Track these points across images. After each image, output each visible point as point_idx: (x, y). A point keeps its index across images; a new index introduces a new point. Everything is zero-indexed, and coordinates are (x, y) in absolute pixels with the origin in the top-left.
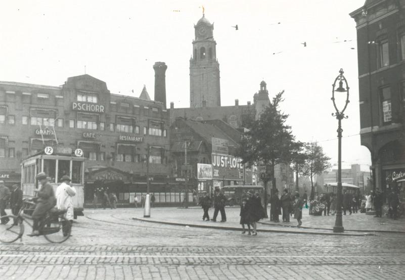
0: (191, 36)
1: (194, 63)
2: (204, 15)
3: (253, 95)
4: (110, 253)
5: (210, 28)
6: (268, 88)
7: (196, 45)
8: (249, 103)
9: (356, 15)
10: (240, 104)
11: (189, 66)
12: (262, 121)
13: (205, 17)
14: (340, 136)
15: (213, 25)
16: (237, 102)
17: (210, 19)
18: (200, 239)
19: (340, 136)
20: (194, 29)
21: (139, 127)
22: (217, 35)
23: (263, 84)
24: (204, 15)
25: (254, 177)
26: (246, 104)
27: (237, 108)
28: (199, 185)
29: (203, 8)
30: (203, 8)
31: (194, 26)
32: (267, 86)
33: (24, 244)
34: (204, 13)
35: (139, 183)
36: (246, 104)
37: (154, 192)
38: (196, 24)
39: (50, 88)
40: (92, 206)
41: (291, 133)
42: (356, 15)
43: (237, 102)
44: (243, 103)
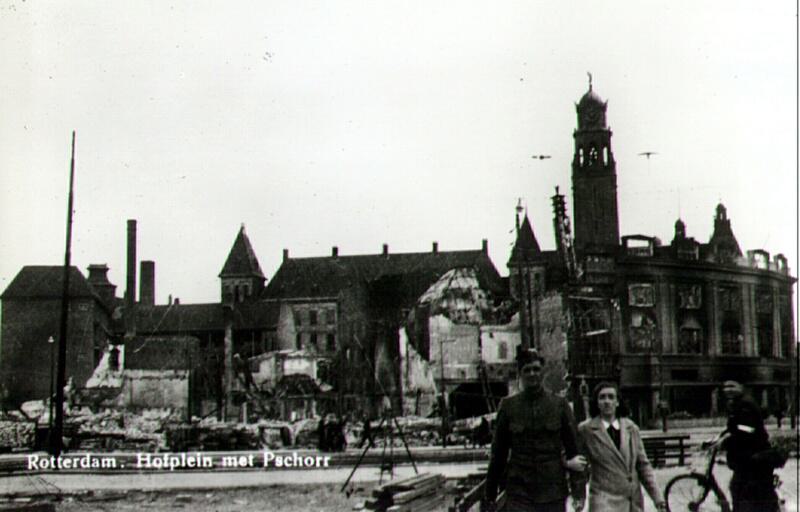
2: (591, 86)
14: (70, 221)
19: (70, 221)
24: (591, 86)
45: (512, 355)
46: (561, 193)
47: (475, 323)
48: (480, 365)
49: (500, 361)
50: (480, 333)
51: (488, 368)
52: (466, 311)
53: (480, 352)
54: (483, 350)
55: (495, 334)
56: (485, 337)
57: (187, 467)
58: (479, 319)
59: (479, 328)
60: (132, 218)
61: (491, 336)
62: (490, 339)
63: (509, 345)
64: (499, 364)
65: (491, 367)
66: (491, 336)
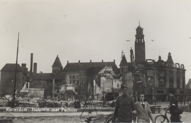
0: (67, 62)
2: (139, 25)
5: (142, 30)
7: (54, 68)
9: (186, 70)
11: (134, 45)
12: (153, 110)
14: (18, 39)
15: (143, 29)
17: (142, 26)
19: (18, 39)
22: (144, 33)
24: (139, 25)
34: (140, 24)
35: (139, 82)
37: (144, 97)
38: (136, 28)
40: (183, 79)
41: (40, 72)
42: (186, 70)
45: (120, 87)
46: (132, 49)
47: (112, 79)
48: (113, 89)
49: (117, 88)
50: (113, 81)
51: (114, 90)
52: (109, 76)
53: (113, 86)
54: (113, 85)
55: (116, 82)
56: (114, 82)
57: (43, 111)
58: (112, 78)
59: (112, 80)
60: (32, 53)
61: (115, 82)
62: (115, 83)
63: (119, 84)
64: (117, 89)
65: (115, 89)
66: (115, 82)
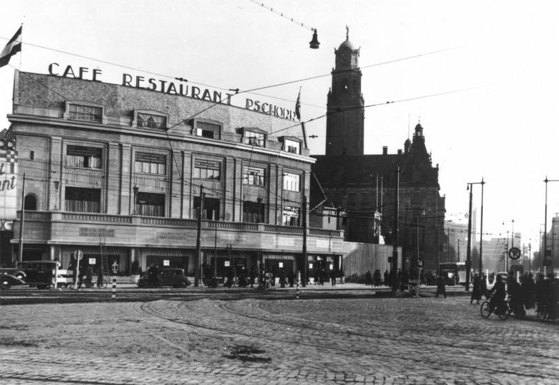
1: (333, 98)
2: (347, 37)
3: (404, 142)
4: (203, 374)
6: (425, 133)
8: (400, 151)
10: (389, 152)
13: (349, 39)
16: (385, 149)
18: (294, 212)
20: (335, 55)
21: (198, 89)
23: (419, 128)
24: (347, 37)
25: (377, 215)
26: (396, 153)
27: (385, 157)
28: (207, 196)
29: (347, 29)
30: (347, 29)
31: (334, 51)
32: (424, 131)
33: (44, 349)
36: (396, 153)
38: (337, 49)
39: (17, 87)
43: (385, 149)
44: (392, 151)
